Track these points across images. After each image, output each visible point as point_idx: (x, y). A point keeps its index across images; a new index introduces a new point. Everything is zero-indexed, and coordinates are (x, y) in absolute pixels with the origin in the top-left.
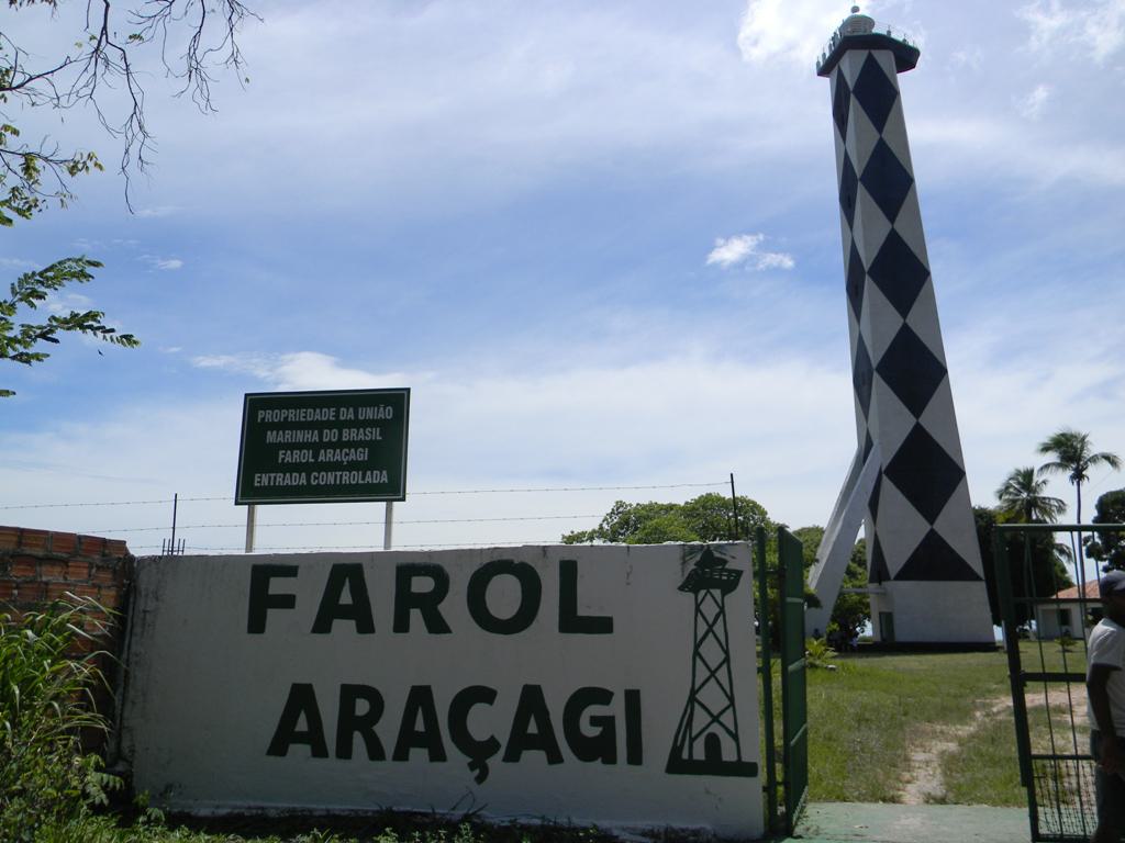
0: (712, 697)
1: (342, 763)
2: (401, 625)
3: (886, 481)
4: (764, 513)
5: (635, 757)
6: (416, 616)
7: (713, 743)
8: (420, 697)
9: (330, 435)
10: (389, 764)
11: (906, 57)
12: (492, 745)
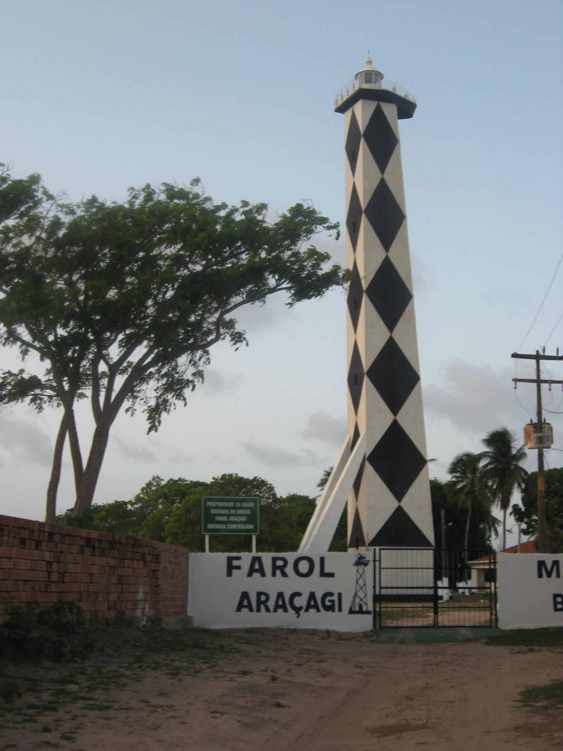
0: (361, 594)
1: (258, 613)
2: (274, 574)
3: (367, 464)
4: (271, 488)
5: (340, 610)
6: (278, 572)
7: (361, 606)
8: (280, 595)
9: (233, 512)
10: (272, 614)
11: (406, 109)
12: (301, 608)
